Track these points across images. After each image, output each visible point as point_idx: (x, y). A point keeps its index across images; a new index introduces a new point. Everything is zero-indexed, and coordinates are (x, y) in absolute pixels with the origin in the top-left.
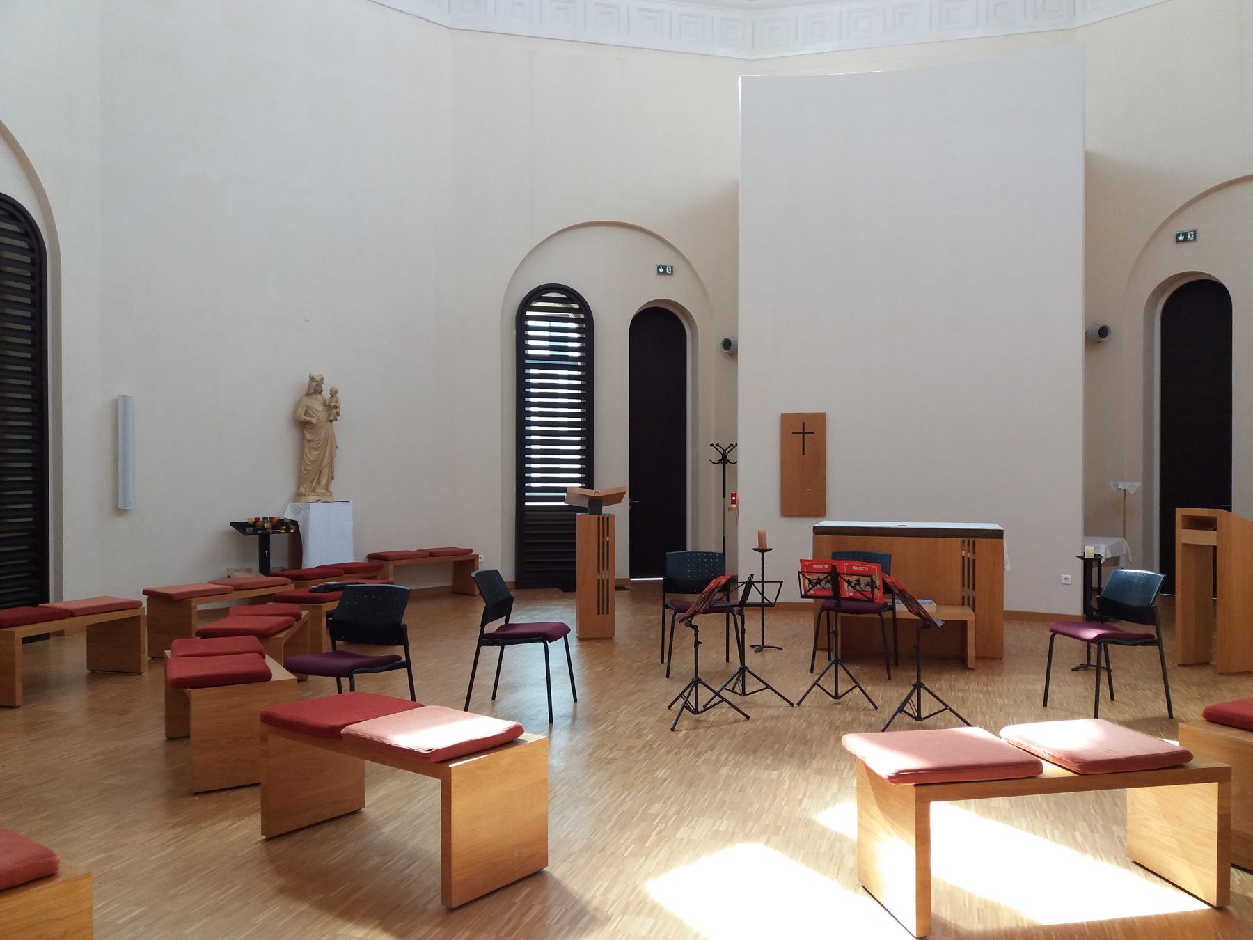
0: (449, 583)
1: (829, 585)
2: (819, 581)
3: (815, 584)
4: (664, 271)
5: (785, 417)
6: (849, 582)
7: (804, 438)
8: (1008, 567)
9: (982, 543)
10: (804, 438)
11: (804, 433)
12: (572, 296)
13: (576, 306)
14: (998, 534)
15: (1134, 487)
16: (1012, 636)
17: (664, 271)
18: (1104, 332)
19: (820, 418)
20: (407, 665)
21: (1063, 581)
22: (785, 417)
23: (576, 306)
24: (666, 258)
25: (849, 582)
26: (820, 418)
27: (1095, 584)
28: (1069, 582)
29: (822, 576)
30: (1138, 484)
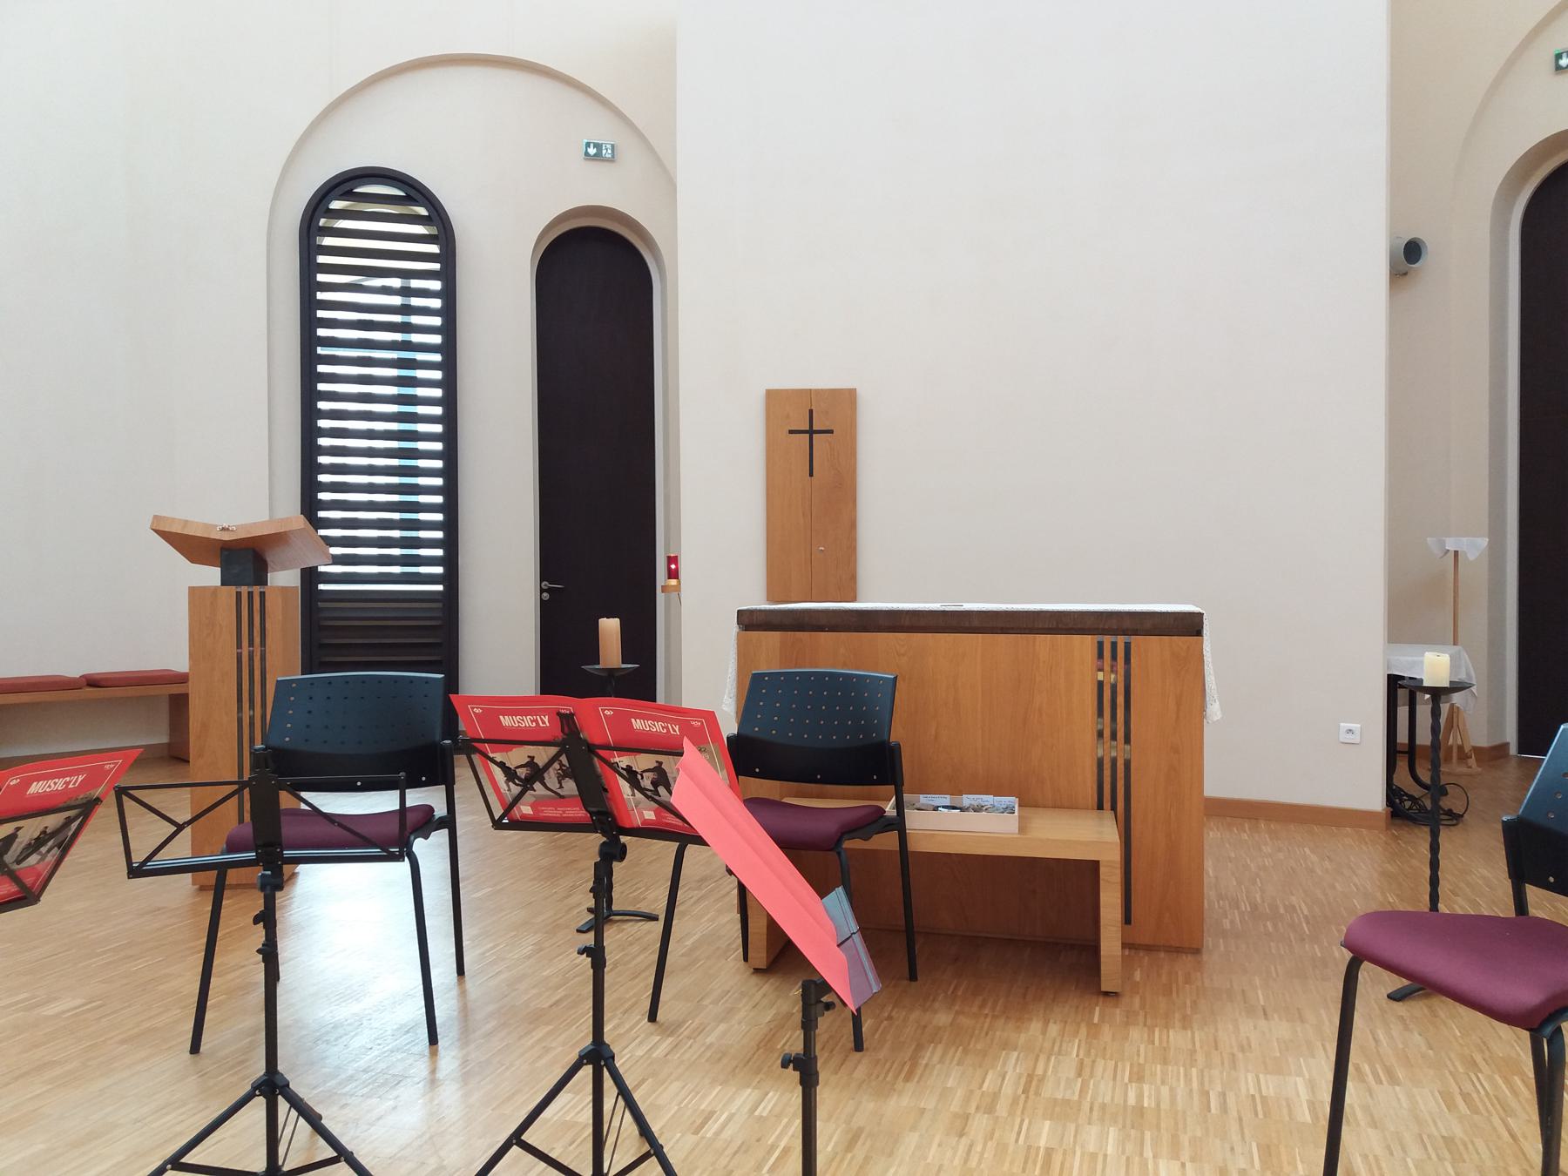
0: (165, 740)
1: (570, 787)
2: (537, 772)
3: (527, 784)
4: (597, 155)
5: (773, 397)
6: (632, 776)
7: (813, 439)
8: (1214, 710)
9: (1149, 649)
10: (813, 439)
11: (811, 432)
12: (414, 191)
13: (422, 211)
14: (1190, 625)
15: (1474, 547)
16: (1229, 869)
17: (597, 155)
18: (1413, 251)
19: (846, 400)
20: (449, 823)
21: (1344, 737)
22: (773, 397)
23: (422, 211)
24: (603, 130)
25: (632, 776)
26: (846, 400)
27: (1402, 737)
28: (1356, 738)
29: (542, 755)
30: (1483, 542)
